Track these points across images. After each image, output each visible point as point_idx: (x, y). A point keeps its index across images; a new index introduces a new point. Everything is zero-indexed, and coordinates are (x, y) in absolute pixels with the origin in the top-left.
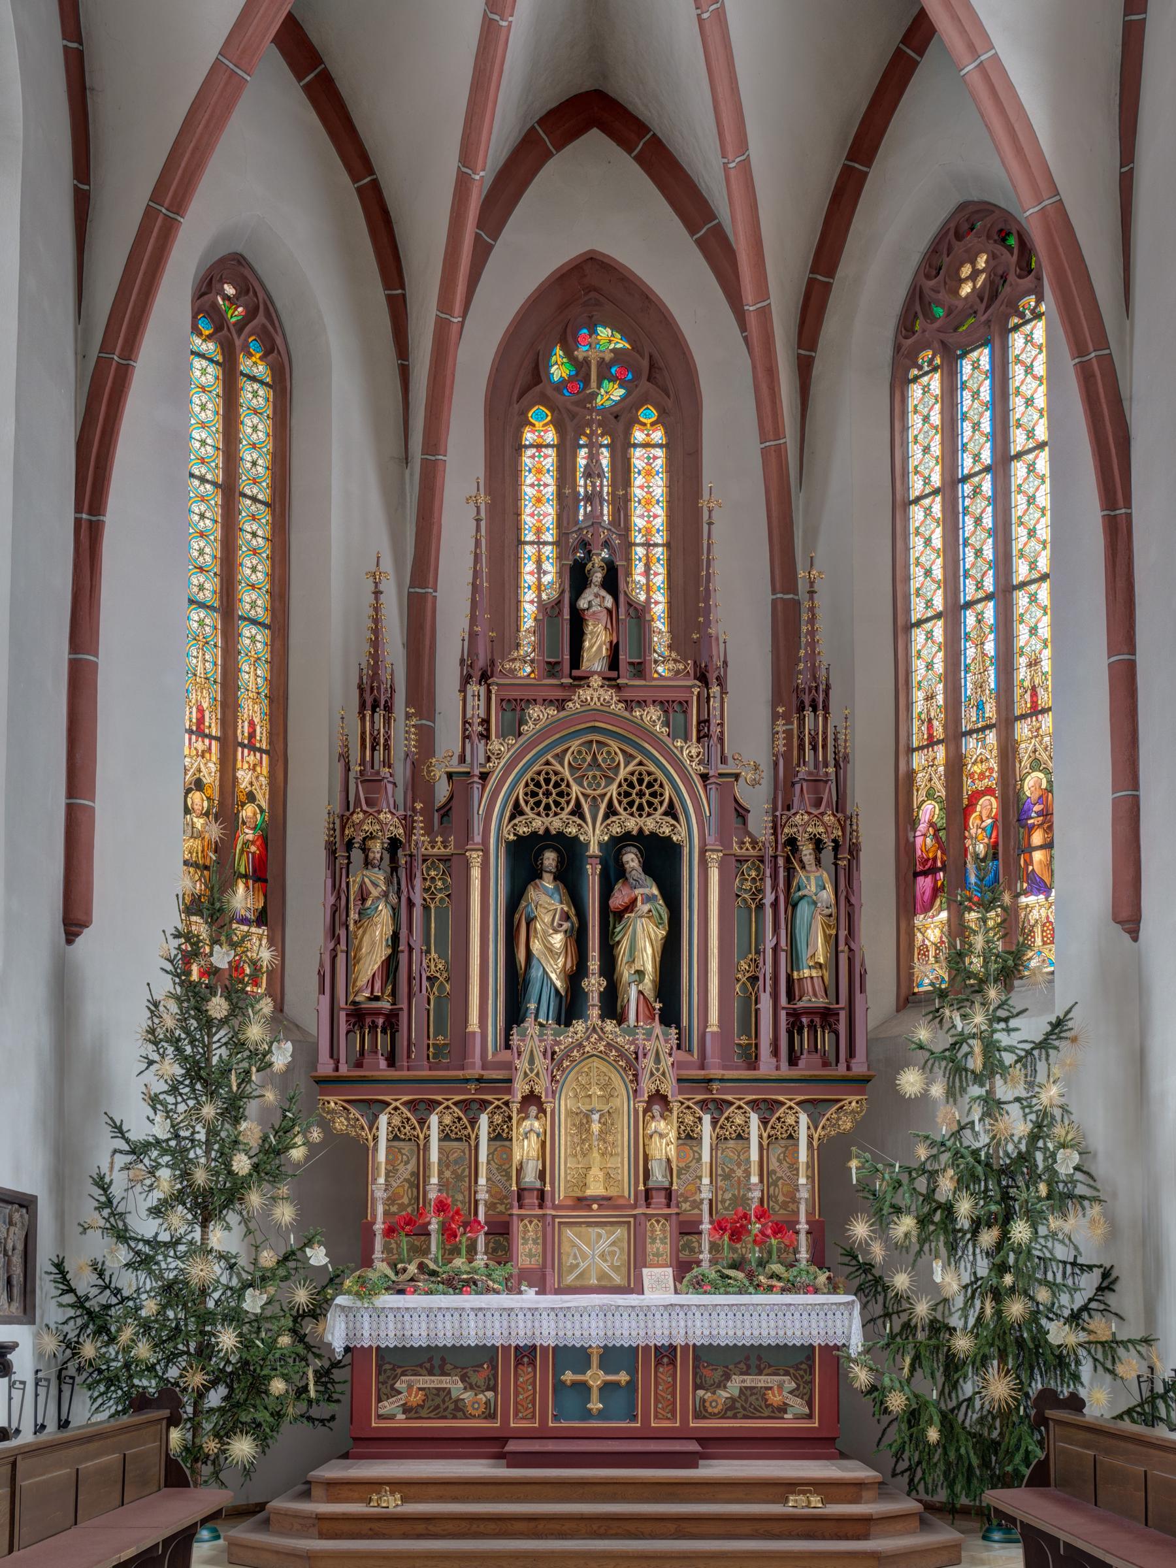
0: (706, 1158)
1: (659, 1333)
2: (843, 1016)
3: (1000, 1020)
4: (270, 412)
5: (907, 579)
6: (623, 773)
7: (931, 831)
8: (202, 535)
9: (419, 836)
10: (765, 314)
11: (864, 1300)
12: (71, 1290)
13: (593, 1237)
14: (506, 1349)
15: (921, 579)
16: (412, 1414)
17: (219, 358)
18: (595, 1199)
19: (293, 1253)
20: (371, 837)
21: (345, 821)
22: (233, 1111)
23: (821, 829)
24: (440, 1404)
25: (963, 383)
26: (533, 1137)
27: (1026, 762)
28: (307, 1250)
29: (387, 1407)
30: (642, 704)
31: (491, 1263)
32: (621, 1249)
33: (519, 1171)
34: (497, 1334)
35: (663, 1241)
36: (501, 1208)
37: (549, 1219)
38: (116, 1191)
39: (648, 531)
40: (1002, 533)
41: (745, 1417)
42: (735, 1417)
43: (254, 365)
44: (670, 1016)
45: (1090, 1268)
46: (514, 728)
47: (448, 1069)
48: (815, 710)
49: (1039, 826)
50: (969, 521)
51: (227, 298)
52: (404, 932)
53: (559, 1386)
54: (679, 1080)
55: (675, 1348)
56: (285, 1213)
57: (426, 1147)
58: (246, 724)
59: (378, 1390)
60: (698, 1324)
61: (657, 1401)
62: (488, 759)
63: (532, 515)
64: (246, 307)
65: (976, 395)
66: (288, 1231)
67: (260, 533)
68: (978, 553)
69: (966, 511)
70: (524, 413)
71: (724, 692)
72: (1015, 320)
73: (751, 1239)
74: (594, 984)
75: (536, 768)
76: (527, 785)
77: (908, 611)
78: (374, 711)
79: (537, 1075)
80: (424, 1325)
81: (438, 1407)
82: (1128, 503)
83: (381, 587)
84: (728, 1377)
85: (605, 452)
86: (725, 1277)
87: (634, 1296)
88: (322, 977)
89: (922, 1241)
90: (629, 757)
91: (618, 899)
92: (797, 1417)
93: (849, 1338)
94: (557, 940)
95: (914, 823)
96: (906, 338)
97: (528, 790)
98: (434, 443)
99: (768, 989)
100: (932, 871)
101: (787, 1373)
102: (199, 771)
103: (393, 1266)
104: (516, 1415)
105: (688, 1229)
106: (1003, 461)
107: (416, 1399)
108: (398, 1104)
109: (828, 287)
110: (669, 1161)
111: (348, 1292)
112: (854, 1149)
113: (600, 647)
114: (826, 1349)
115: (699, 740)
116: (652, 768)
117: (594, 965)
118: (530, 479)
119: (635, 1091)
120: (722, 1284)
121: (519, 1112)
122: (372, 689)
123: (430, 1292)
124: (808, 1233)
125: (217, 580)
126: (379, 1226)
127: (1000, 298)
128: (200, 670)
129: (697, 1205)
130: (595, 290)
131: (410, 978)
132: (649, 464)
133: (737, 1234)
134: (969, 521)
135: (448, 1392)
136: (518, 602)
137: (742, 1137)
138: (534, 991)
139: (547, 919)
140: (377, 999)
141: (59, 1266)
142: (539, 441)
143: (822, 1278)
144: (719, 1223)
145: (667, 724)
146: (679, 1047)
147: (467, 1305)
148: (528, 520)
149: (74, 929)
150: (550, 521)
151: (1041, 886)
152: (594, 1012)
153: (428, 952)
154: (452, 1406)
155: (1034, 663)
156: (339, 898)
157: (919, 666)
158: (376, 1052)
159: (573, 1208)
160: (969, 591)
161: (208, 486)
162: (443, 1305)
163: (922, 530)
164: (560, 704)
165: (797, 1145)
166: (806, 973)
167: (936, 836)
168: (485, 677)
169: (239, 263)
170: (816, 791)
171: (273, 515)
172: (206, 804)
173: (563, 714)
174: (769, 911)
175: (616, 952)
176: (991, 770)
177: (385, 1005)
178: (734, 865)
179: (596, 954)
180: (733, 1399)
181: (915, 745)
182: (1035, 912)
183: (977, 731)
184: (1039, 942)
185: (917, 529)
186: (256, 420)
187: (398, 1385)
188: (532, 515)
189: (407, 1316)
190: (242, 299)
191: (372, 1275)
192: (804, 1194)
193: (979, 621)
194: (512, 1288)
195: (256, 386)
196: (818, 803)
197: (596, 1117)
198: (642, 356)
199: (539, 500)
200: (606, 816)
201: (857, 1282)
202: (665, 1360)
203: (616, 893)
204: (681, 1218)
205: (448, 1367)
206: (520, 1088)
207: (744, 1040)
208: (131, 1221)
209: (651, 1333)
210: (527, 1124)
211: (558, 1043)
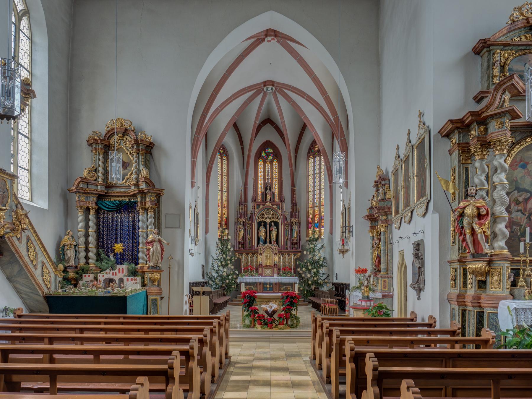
0: (281, 261)
5: (309, 185)
9: (247, 221)
30: (274, 205)
43: (225, 158)
44: (277, 243)
46: (258, 208)
50: (316, 179)
57: (248, 259)
74: (268, 240)
84: (283, 286)
90: (272, 212)
91: (271, 229)
94: (264, 234)
95: (309, 217)
105: (279, 269)
117: (268, 237)
118: (260, 181)
120: (283, 276)
126: (243, 268)
133: (285, 270)
134: (316, 179)
137: (286, 258)
138: (261, 240)
148: (259, 175)
151: (323, 227)
157: (310, 197)
160: (316, 189)
164: (264, 205)
168: (255, 201)
177: (243, 242)
178: (285, 225)
194: (258, 276)
206: (259, 252)
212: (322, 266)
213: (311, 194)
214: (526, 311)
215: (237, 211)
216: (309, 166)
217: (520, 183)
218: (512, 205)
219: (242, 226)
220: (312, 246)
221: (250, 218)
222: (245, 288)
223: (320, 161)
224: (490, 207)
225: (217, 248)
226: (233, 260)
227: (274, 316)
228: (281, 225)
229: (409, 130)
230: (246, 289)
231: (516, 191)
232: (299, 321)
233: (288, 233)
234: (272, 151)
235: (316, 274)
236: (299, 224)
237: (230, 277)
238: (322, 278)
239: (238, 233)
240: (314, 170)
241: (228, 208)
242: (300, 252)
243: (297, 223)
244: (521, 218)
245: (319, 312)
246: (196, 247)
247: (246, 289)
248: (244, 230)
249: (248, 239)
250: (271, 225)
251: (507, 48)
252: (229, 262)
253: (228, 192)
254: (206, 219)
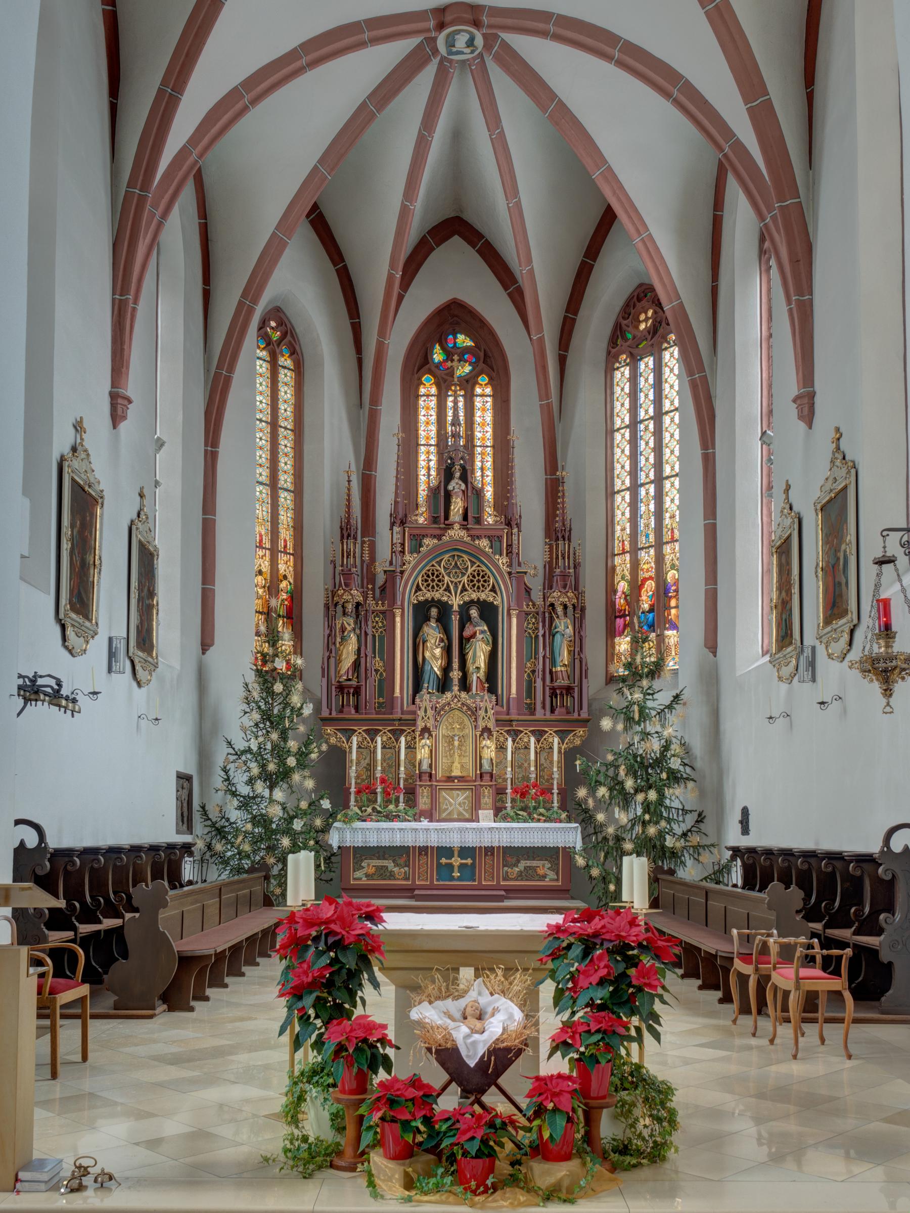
0: (509, 758)
1: (486, 840)
2: (576, 689)
3: (649, 694)
4: (293, 384)
5: (613, 469)
6: (470, 571)
7: (623, 596)
8: (261, 448)
9: (370, 601)
10: (541, 340)
11: (585, 826)
12: (209, 819)
13: (455, 795)
14: (414, 848)
15: (620, 470)
16: (370, 878)
17: (268, 359)
18: (456, 777)
19: (314, 802)
20: (347, 602)
21: (334, 594)
22: (284, 737)
23: (567, 600)
24: (382, 872)
25: (641, 373)
26: (427, 748)
27: (668, 565)
28: (321, 801)
29: (358, 874)
30: (479, 537)
31: (407, 807)
32: (469, 801)
33: (420, 764)
34: (410, 840)
35: (488, 797)
36: (411, 781)
37: (434, 787)
38: (231, 773)
39: (483, 439)
40: (658, 449)
41: (527, 880)
42: (522, 880)
43: (285, 361)
44: (492, 690)
45: (691, 811)
46: (416, 549)
47: (384, 714)
48: (564, 540)
49: (674, 597)
53: (439, 865)
54: (497, 721)
55: (494, 848)
56: (310, 784)
57: (375, 752)
58: (283, 541)
59: (354, 866)
60: (505, 836)
61: (485, 873)
62: (404, 564)
63: (424, 431)
64: (281, 332)
65: (646, 380)
66: (311, 792)
67: (288, 445)
68: (647, 459)
69: (641, 437)
70: (420, 379)
71: (519, 531)
72: (665, 345)
73: (530, 797)
74: (456, 675)
75: (427, 568)
76: (423, 576)
77: (613, 485)
78: (348, 539)
79: (428, 718)
80: (375, 836)
81: (382, 874)
82: (714, 447)
83: (351, 479)
84: (518, 861)
85: (461, 399)
86: (517, 814)
87: (475, 823)
88: (323, 670)
89: (611, 798)
90: (473, 563)
91: (467, 633)
92: (551, 880)
93: (575, 843)
94: (438, 652)
95: (615, 591)
96: (613, 348)
97: (424, 578)
98: (375, 400)
99: (540, 676)
100: (624, 616)
101: (546, 860)
102: (260, 565)
103: (360, 808)
104: (419, 879)
105: (500, 792)
106: (658, 417)
107: (371, 871)
108: (360, 731)
109: (574, 320)
110: (491, 760)
111: (340, 821)
112: (578, 756)
113: (459, 509)
114: (564, 848)
115: (507, 556)
116: (484, 568)
117: (456, 665)
118: (423, 412)
119: (475, 726)
120: (516, 818)
121: (419, 736)
122: (347, 529)
123: (378, 821)
124: (558, 794)
125: (268, 470)
127: (659, 333)
128: (260, 516)
129: (505, 780)
130: (457, 316)
131: (366, 670)
132: (483, 405)
133: (523, 795)
135: (387, 867)
136: (417, 475)
137: (527, 748)
138: (426, 677)
139: (433, 641)
140: (350, 680)
141: (203, 807)
142: (428, 393)
143: (564, 815)
144: (515, 789)
145: (491, 547)
146: (497, 704)
147: (396, 827)
148: (422, 433)
149: (206, 647)
150: (433, 434)
151: (674, 627)
152: (456, 688)
153: (375, 657)
154: (388, 874)
155: (672, 517)
156: (331, 631)
157: (618, 513)
158: (350, 705)
159: (446, 782)
160: (642, 478)
161: (263, 424)
162: (384, 827)
163: (620, 445)
164: (439, 537)
165: (553, 752)
166: (559, 669)
167: (625, 598)
168: (403, 523)
169: (278, 311)
170: (564, 581)
171: (295, 436)
172: (264, 582)
173: (440, 542)
174: (541, 639)
175: (466, 657)
176: (652, 568)
177: (354, 683)
178: (524, 616)
179: (457, 660)
180: (521, 872)
181: (616, 553)
182: (672, 639)
183: (646, 548)
184: (673, 653)
185: (618, 444)
186: (286, 388)
187: (363, 864)
188: (424, 431)
189: (367, 832)
190: (279, 328)
191: (350, 813)
192: (556, 776)
193: (647, 494)
195: (286, 371)
196: (565, 587)
197: (456, 738)
198: (480, 350)
199: (428, 423)
200: (462, 592)
201: (581, 817)
202: (489, 853)
203: (466, 629)
204: (497, 787)
205: (387, 856)
206: (420, 724)
207: (528, 701)
208: (238, 787)
209: (482, 840)
210: (423, 741)
211: (438, 703)
212: (675, 778)
213: (622, 502)
215: (333, 562)
216: (616, 395)
219: (349, 623)
220: (638, 696)
221: (383, 589)
223: (658, 370)
225: (245, 707)
226: (313, 756)
227: (501, 1081)
228: (509, 615)
229: (837, 430)
232: (672, 1113)
233: (536, 652)
234: (469, 343)
235: (654, 810)
236: (578, 612)
237: (298, 825)
238: (678, 830)
239: (337, 650)
240: (634, 409)
241: (298, 555)
242: (584, 722)
243: (570, 609)
245: (721, 1001)
246: (140, 694)
249: (377, 671)
250: (469, 618)
252: (291, 761)
253: (298, 491)
254: (204, 590)
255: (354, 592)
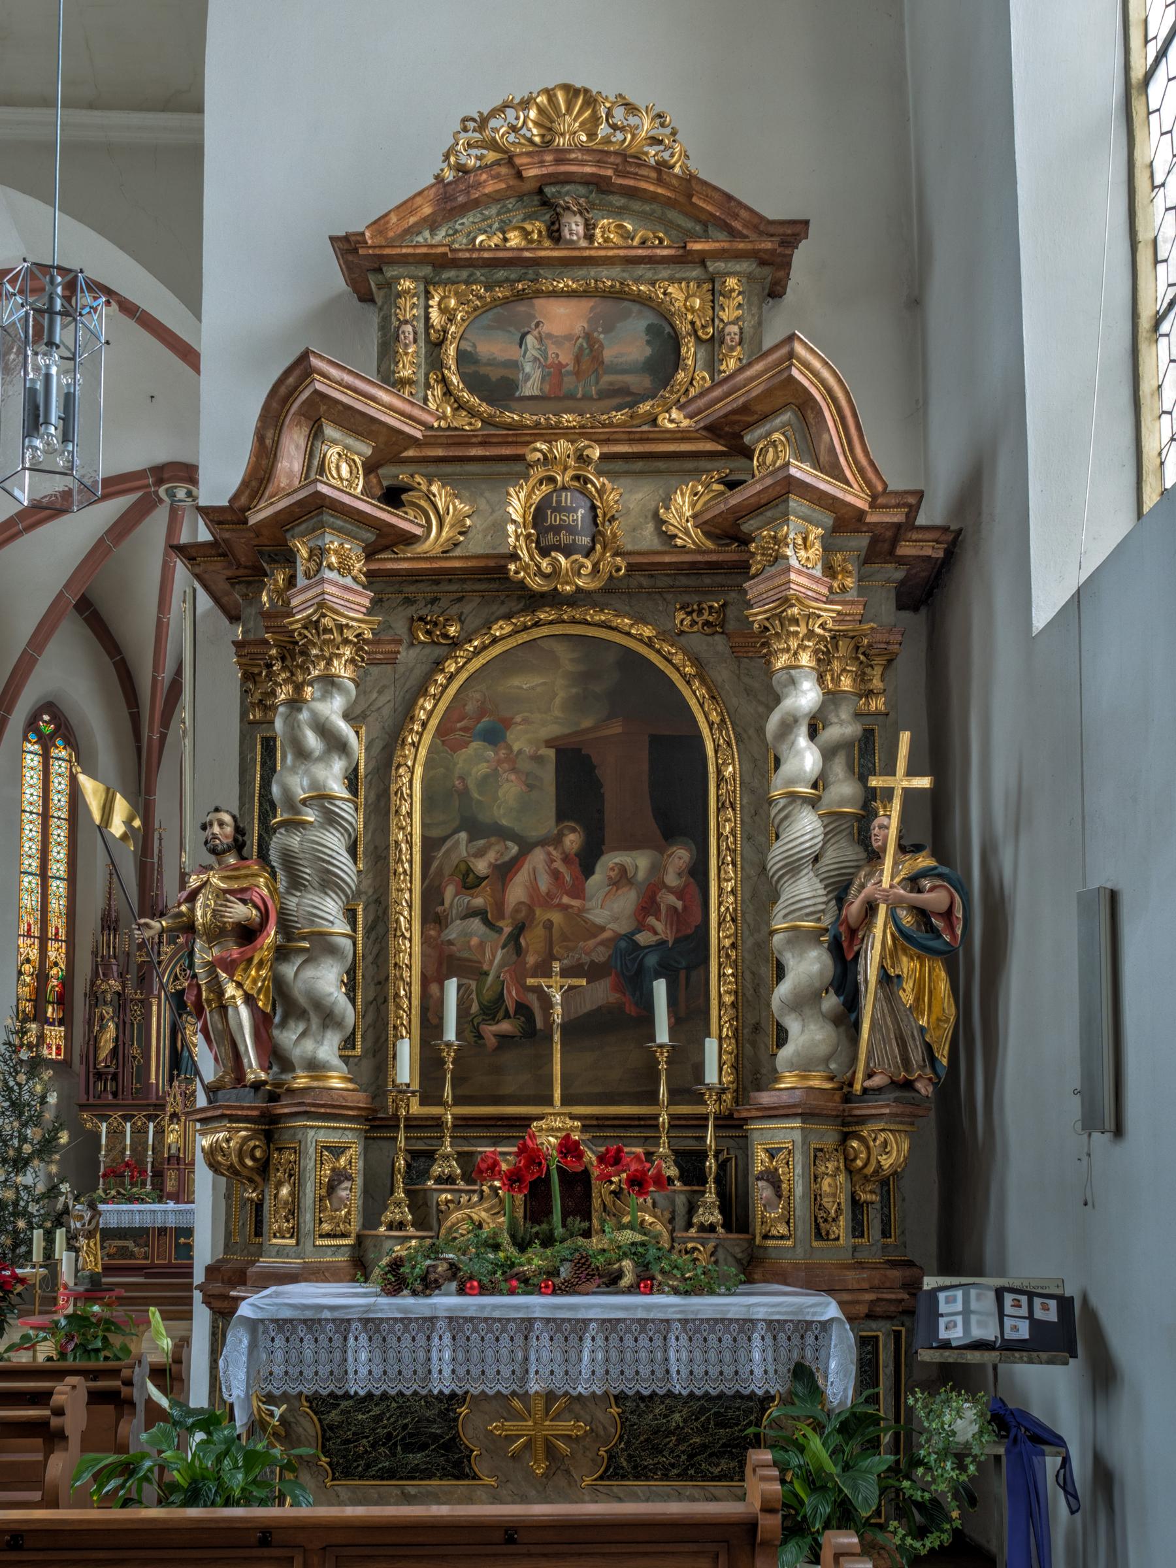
33: (169, 1149)
51: (44, 722)
52: (121, 1035)
53: (177, 1245)
107: (113, 1250)
206: (169, 1110)
214: (294, 1331)
217: (479, 802)
218: (449, 892)
219: (108, 1011)
222: (102, 1248)
224: (364, 898)
230: (109, 1255)
231: (463, 835)
244: (482, 945)
247: (109, 1255)
248: (117, 1026)
249: (134, 1057)
251: (451, 274)
253: (72, 879)
255: (112, 982)
